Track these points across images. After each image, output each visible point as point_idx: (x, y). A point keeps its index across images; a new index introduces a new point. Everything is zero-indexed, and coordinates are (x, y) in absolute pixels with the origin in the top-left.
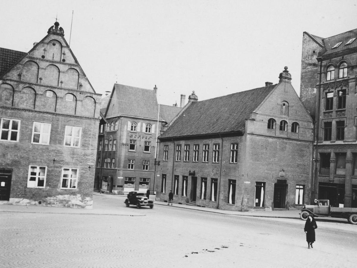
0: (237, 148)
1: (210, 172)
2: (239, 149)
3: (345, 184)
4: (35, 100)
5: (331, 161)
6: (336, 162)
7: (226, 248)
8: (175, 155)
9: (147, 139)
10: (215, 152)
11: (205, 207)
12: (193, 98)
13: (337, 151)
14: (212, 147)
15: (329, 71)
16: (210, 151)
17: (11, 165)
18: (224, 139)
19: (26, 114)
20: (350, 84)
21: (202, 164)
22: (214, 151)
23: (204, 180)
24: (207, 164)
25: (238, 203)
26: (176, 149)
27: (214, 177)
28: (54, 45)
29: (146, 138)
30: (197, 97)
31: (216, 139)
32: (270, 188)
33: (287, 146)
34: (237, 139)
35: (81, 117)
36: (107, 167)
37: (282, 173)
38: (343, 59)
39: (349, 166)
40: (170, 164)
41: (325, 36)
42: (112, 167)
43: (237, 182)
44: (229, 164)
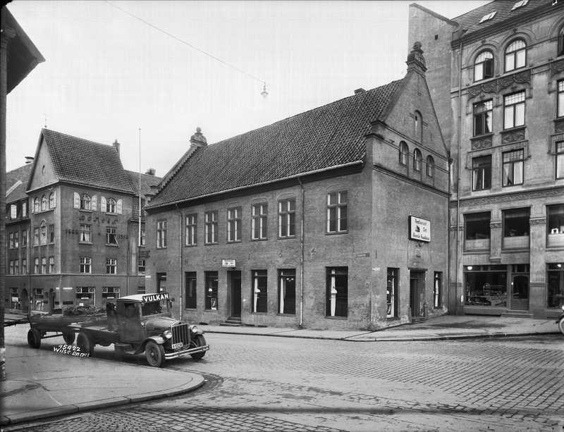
1: (274, 257)
3: (528, 266)
5: (494, 224)
8: (184, 235)
9: (111, 222)
11: (266, 327)
12: (198, 140)
13: (507, 206)
14: (276, 207)
16: (270, 216)
18: (305, 186)
21: (252, 243)
22: (279, 214)
24: (264, 243)
25: (355, 313)
26: (184, 223)
27: (284, 267)
29: (109, 222)
30: (205, 139)
31: (284, 190)
36: (40, 272)
38: (516, 34)
42: (50, 272)
43: (349, 271)
44: (327, 235)
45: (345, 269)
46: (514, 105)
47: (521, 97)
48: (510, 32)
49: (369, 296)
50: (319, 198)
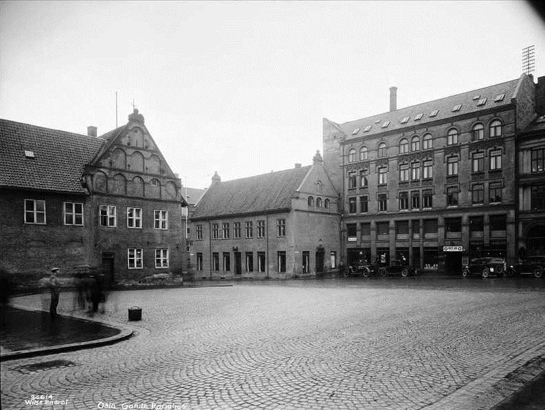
0: (239, 226)
1: (255, 245)
2: (286, 224)
4: (126, 187)
6: (361, 230)
7: (131, 340)
10: (198, 231)
12: (216, 179)
13: (363, 221)
15: (476, 159)
17: (113, 249)
19: (120, 200)
20: (390, 163)
23: (250, 255)
28: (136, 132)
32: (313, 256)
33: (323, 219)
34: (283, 216)
35: (166, 201)
37: (321, 243)
39: (373, 233)
40: (206, 242)
41: (340, 123)
45: (285, 252)
46: (453, 163)
47: (499, 152)
48: (450, 124)
49: (293, 265)
50: (273, 222)
